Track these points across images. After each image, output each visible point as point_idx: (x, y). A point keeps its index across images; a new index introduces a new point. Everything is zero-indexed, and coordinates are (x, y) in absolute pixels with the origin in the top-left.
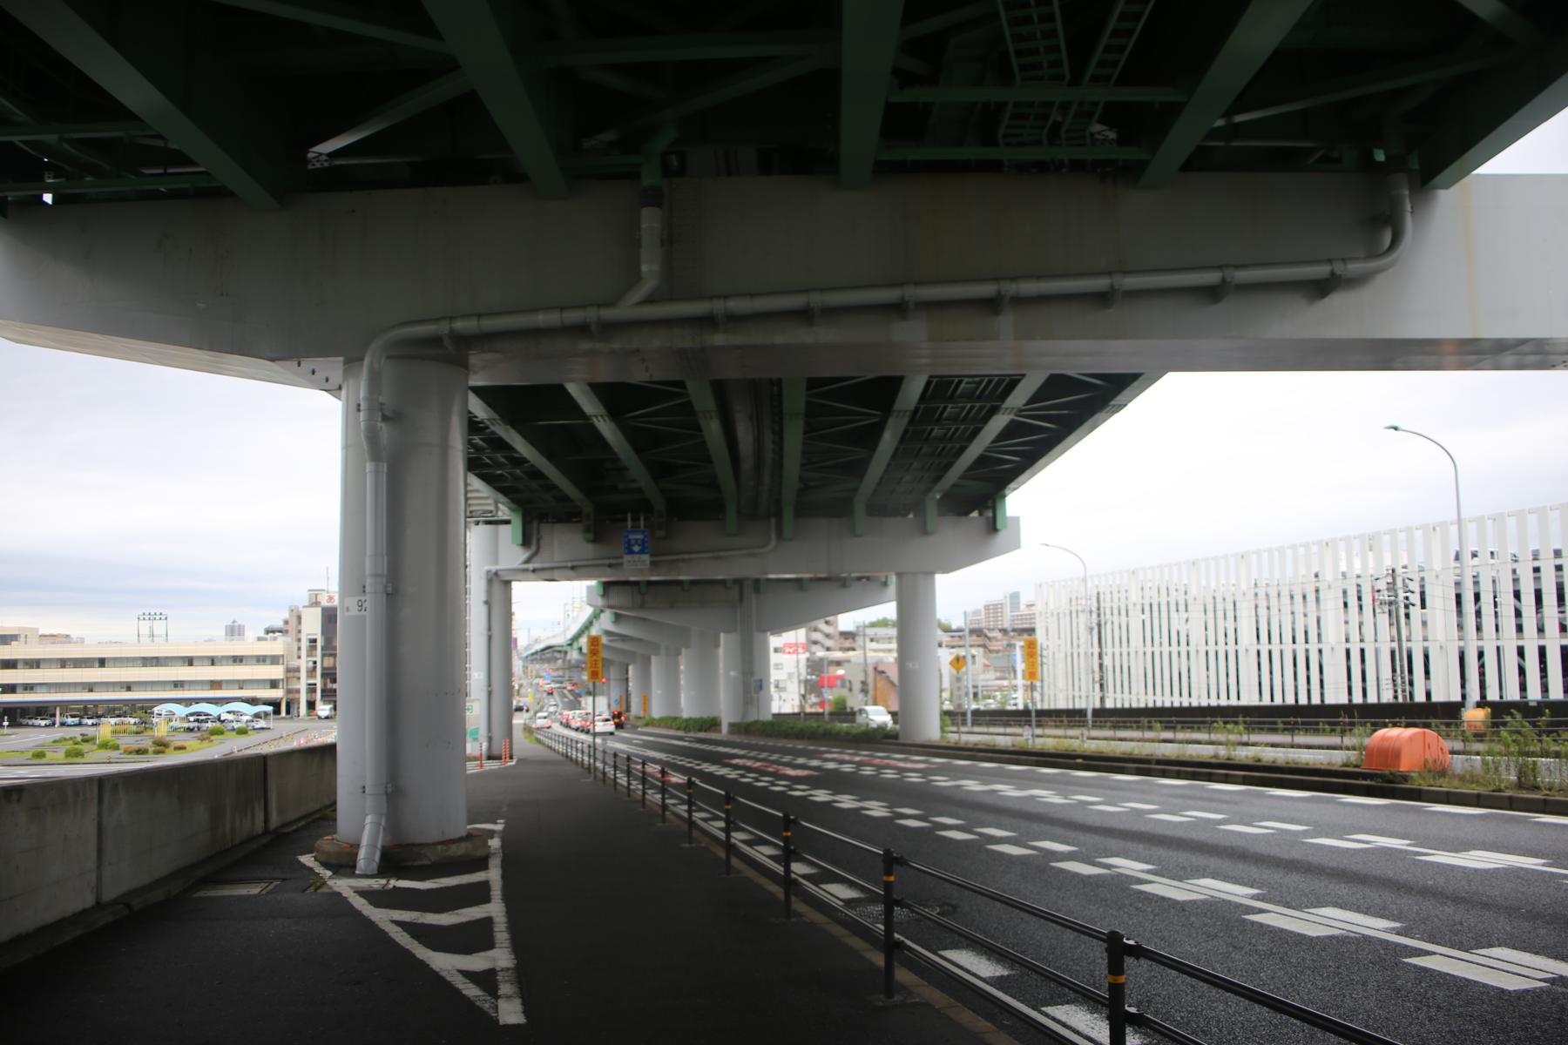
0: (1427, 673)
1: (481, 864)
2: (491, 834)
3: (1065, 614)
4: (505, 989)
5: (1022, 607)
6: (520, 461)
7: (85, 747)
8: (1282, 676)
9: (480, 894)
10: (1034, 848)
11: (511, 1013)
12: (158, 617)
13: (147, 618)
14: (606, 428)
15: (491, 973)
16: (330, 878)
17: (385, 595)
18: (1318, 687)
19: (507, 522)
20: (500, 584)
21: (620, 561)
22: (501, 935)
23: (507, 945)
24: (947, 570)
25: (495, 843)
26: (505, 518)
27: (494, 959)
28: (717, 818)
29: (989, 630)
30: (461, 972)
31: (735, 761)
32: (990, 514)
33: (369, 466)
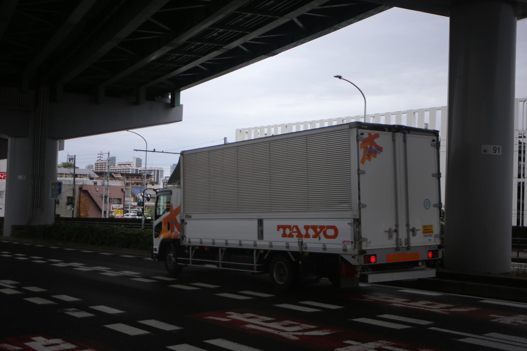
5: (116, 165)
10: (230, 318)
29: (115, 173)
31: (367, 298)
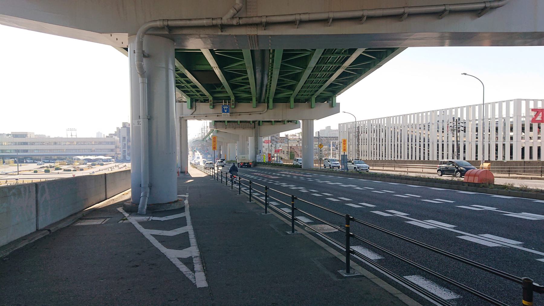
0: (464, 152)
1: (182, 209)
2: (185, 198)
3: (244, 157)
4: (198, 267)
6: (189, 82)
7: (50, 169)
8: (416, 152)
9: (182, 222)
11: (201, 281)
12: (73, 130)
13: (70, 130)
14: (218, 72)
15: (191, 258)
16: (128, 216)
17: (147, 119)
18: (413, 155)
19: (186, 102)
20: (183, 122)
21: (221, 114)
22: (193, 240)
23: (195, 245)
24: (318, 119)
25: (186, 202)
26: (185, 100)
27: (191, 252)
28: (262, 195)
30: (179, 258)
32: (331, 102)
33: (140, 79)
